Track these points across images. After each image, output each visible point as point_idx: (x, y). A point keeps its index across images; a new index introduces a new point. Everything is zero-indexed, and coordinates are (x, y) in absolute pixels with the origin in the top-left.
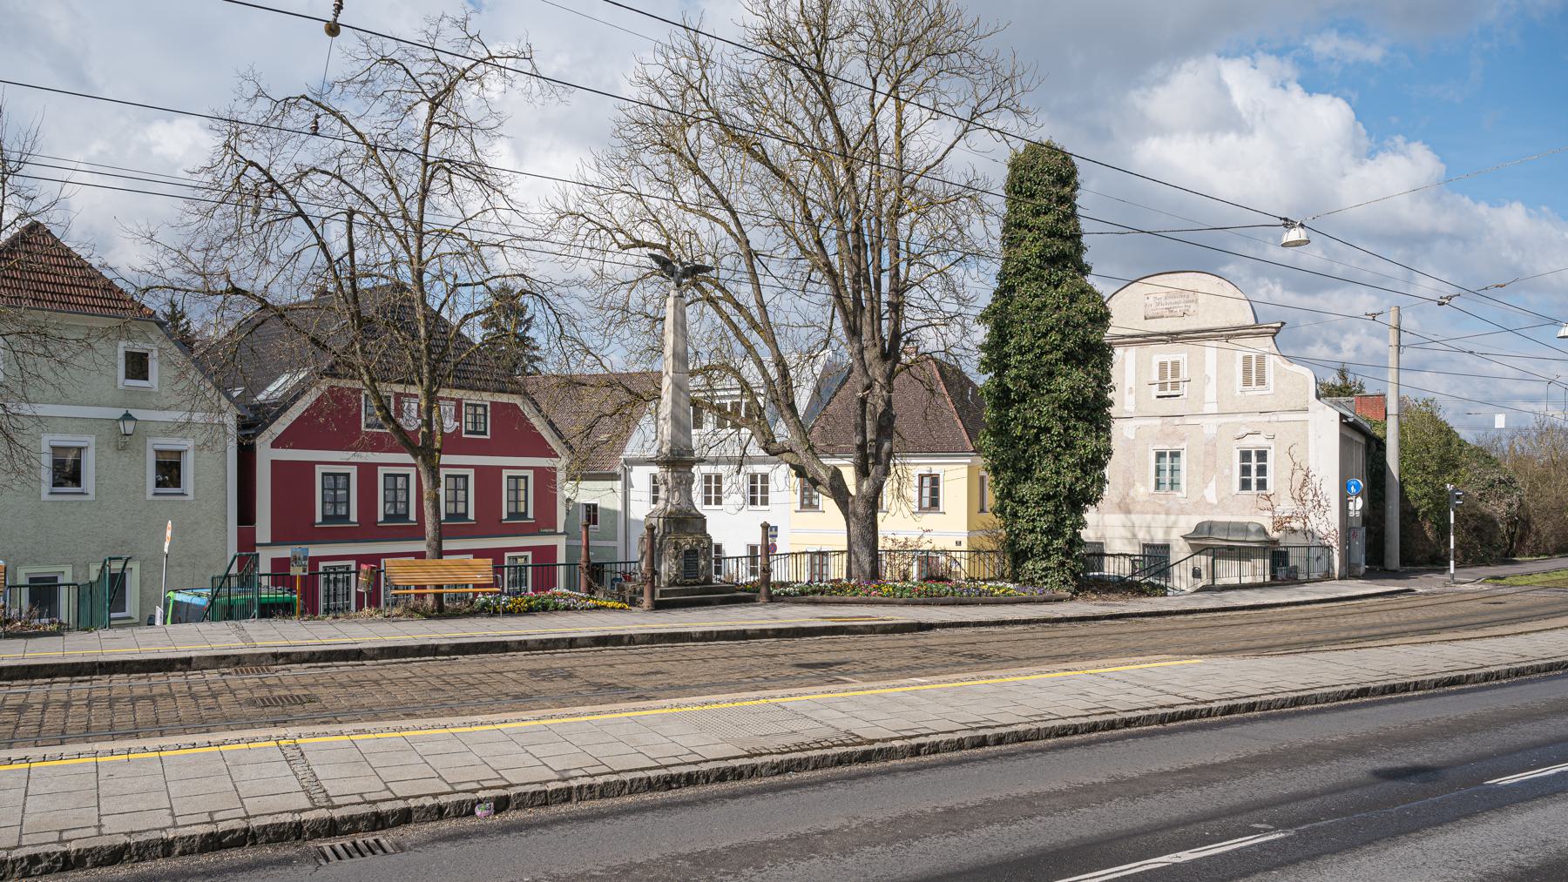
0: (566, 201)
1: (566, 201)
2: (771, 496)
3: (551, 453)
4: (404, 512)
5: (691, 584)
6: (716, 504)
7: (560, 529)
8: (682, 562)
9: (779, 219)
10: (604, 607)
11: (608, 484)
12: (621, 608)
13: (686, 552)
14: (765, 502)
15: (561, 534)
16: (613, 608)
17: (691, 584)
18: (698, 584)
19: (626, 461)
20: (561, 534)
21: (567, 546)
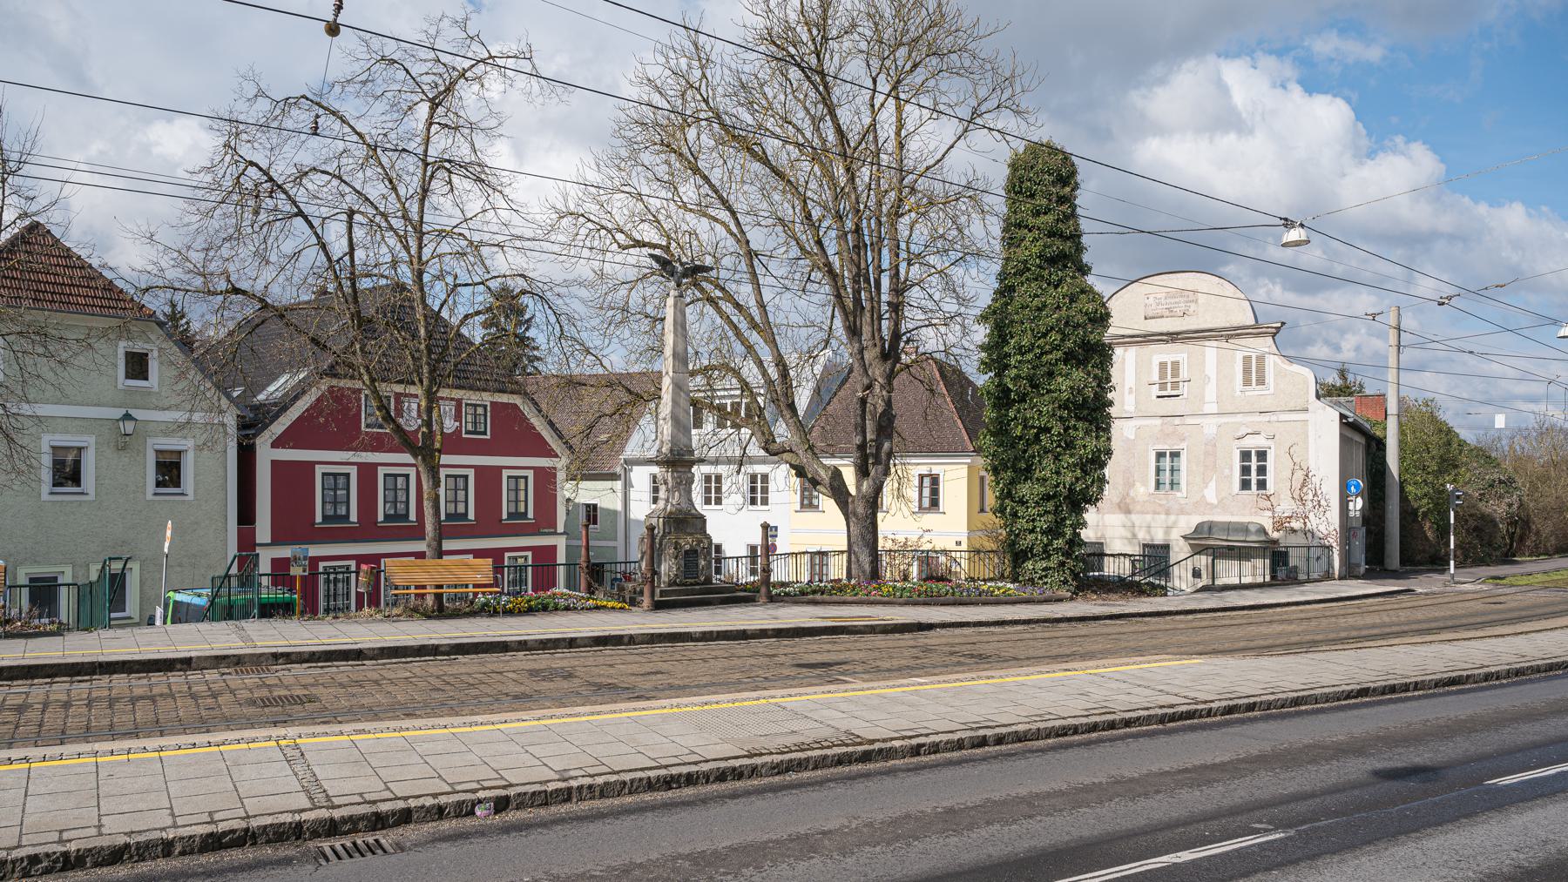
2: (771, 496)
4: (404, 512)
5: (691, 584)
6: (716, 504)
7: (560, 529)
8: (682, 562)
10: (604, 607)
11: (608, 484)
12: (621, 608)
13: (686, 552)
14: (765, 502)
15: (561, 534)
16: (613, 608)
17: (691, 584)
18: (698, 584)
19: (626, 461)
20: (561, 534)
21: (567, 546)
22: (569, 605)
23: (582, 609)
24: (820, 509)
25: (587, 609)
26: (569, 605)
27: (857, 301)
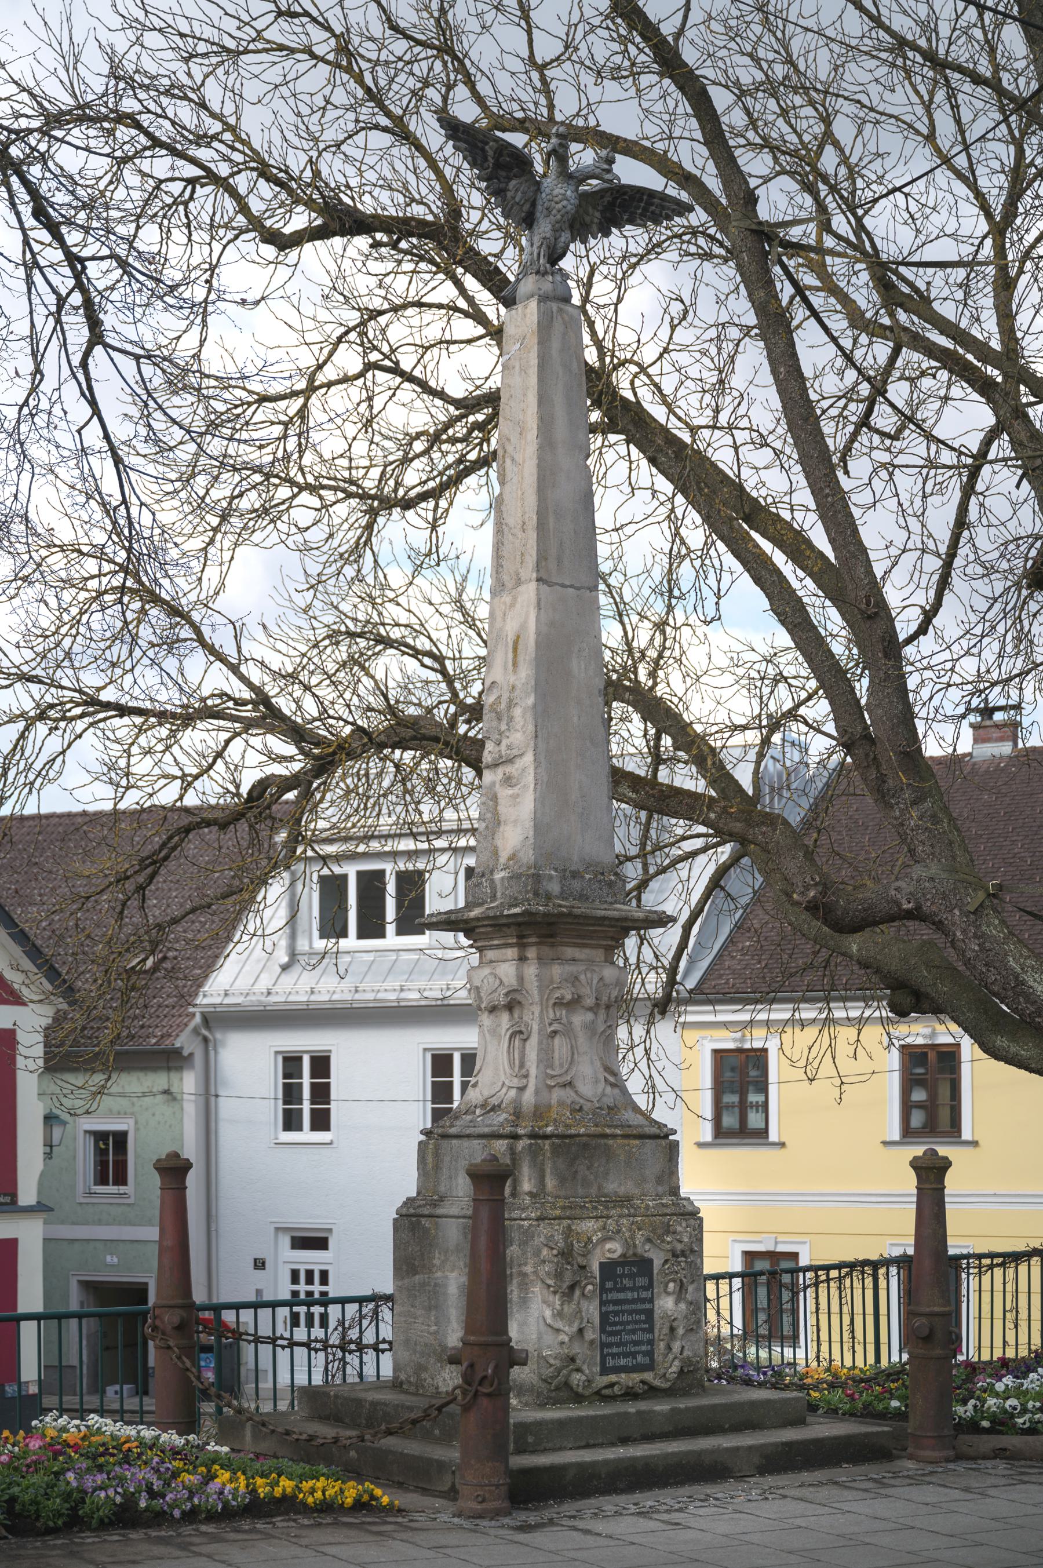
0: (72, 60)
1: (72, 60)
2: (336, 1110)
3: (684, 209)
4: (763, 1126)
5: (630, 1395)
6: (314, 1127)
7: (27, 1194)
8: (592, 1310)
9: (118, 881)
10: (287, 1505)
11: (158, 1080)
12: (360, 1506)
13: (608, 1268)
14: (321, 1121)
15: (29, 1210)
16: (326, 1507)
17: (630, 1395)
18: (652, 1392)
19: (207, 1020)
20: (29, 1210)
21: (46, 1240)
22: (130, 1500)
23: (191, 1516)
24: (773, 1137)
25: (212, 1517)
26: (130, 1500)
27: (151, 864)
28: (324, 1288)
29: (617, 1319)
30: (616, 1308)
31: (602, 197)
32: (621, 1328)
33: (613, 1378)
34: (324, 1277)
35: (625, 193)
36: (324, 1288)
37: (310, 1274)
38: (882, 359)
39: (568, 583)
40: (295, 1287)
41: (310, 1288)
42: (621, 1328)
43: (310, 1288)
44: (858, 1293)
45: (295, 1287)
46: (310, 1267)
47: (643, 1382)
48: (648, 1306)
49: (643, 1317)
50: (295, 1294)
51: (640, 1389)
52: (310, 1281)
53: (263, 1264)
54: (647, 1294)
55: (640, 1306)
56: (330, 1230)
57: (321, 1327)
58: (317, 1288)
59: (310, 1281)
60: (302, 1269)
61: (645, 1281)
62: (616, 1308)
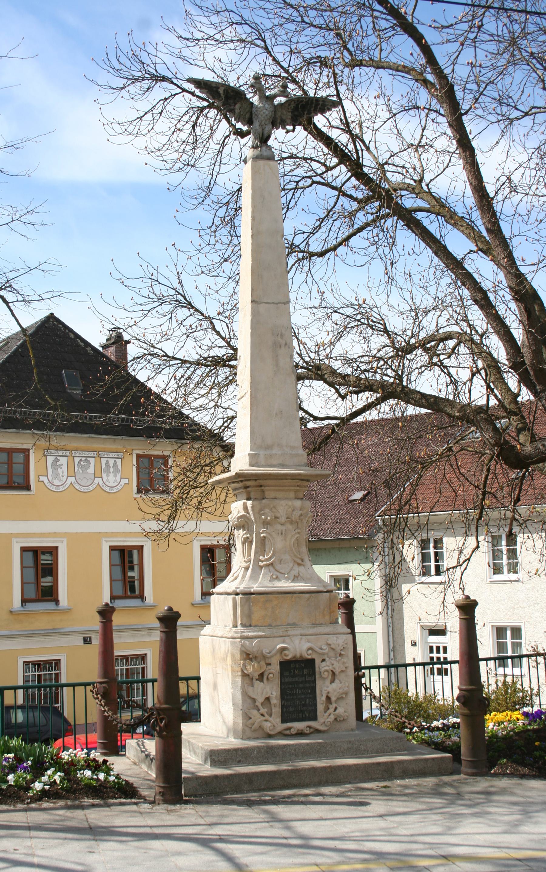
17: (300, 734)
28: (445, 655)
29: (291, 692)
30: (290, 686)
31: (289, 105)
32: (294, 697)
33: (289, 725)
34: (445, 650)
35: (302, 101)
36: (445, 655)
37: (438, 648)
38: (333, 164)
39: (270, 301)
40: (431, 655)
41: (438, 655)
42: (294, 697)
43: (438, 655)
44: (533, 671)
45: (431, 655)
46: (445, 645)
47: (310, 727)
48: (312, 685)
49: (309, 691)
50: (432, 658)
51: (308, 731)
52: (438, 651)
53: (415, 643)
54: (311, 679)
55: (307, 685)
56: (493, 626)
57: (431, 674)
58: (442, 655)
59: (438, 651)
60: (434, 646)
61: (310, 671)
62: (290, 686)
